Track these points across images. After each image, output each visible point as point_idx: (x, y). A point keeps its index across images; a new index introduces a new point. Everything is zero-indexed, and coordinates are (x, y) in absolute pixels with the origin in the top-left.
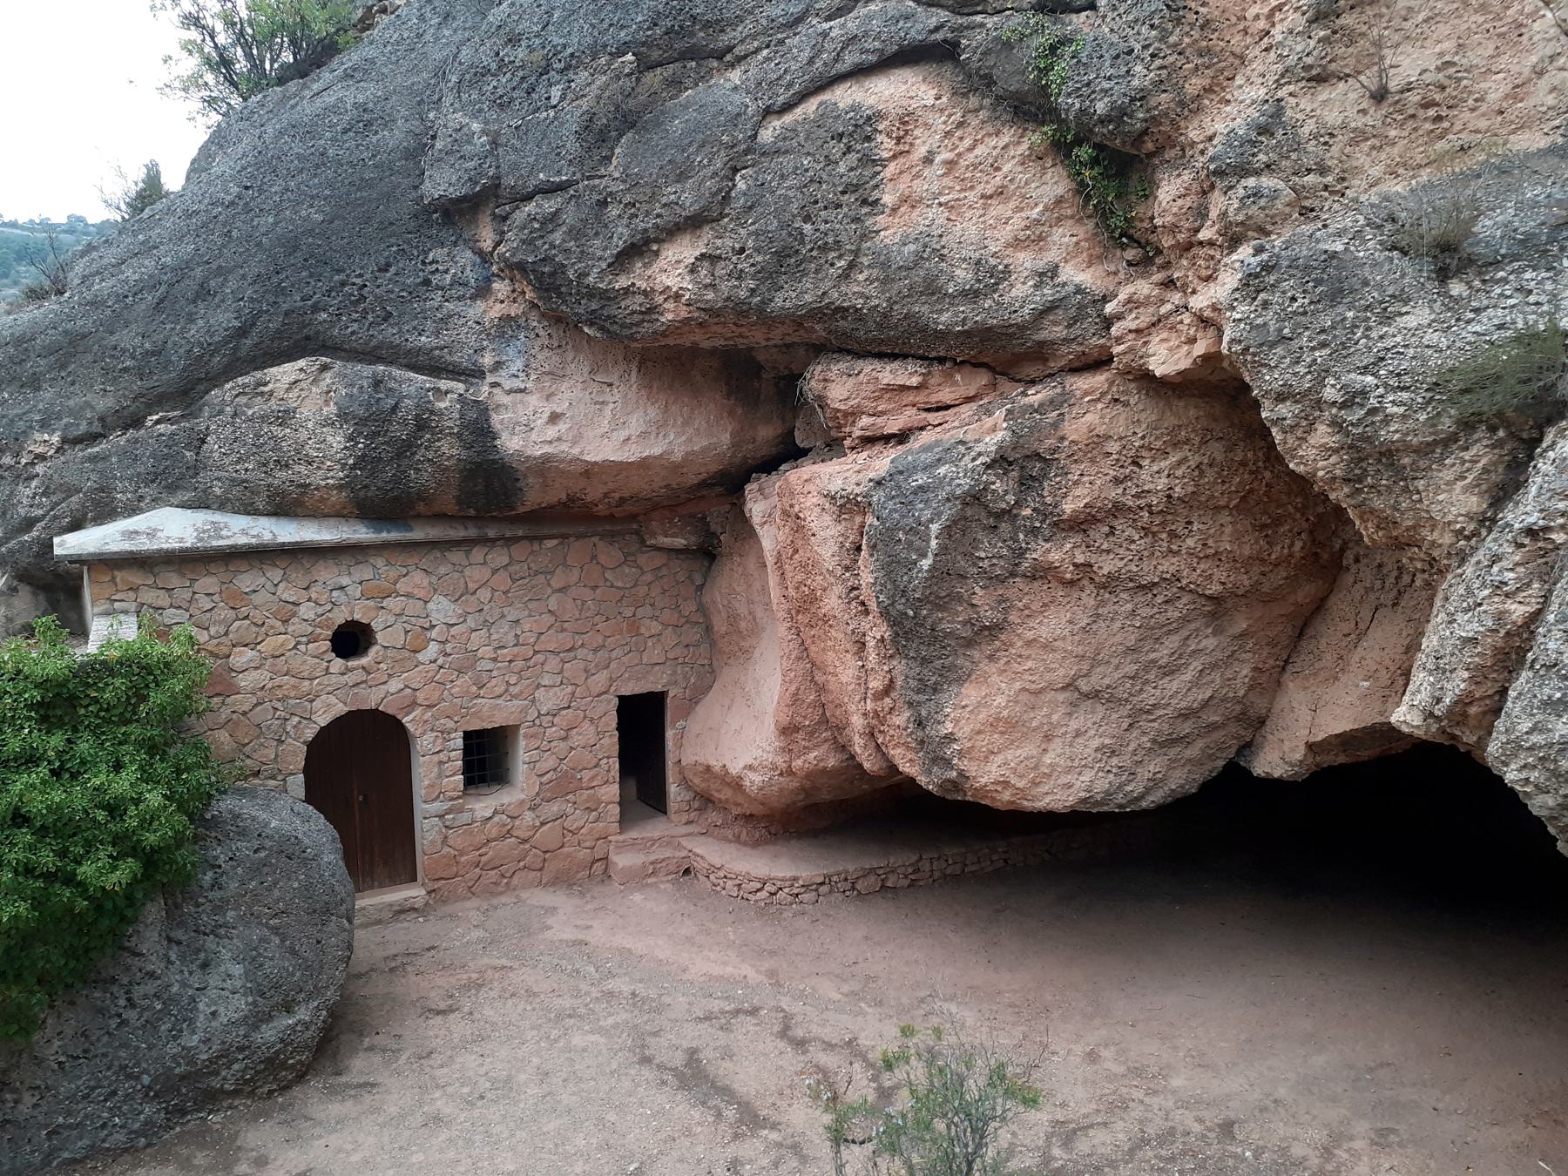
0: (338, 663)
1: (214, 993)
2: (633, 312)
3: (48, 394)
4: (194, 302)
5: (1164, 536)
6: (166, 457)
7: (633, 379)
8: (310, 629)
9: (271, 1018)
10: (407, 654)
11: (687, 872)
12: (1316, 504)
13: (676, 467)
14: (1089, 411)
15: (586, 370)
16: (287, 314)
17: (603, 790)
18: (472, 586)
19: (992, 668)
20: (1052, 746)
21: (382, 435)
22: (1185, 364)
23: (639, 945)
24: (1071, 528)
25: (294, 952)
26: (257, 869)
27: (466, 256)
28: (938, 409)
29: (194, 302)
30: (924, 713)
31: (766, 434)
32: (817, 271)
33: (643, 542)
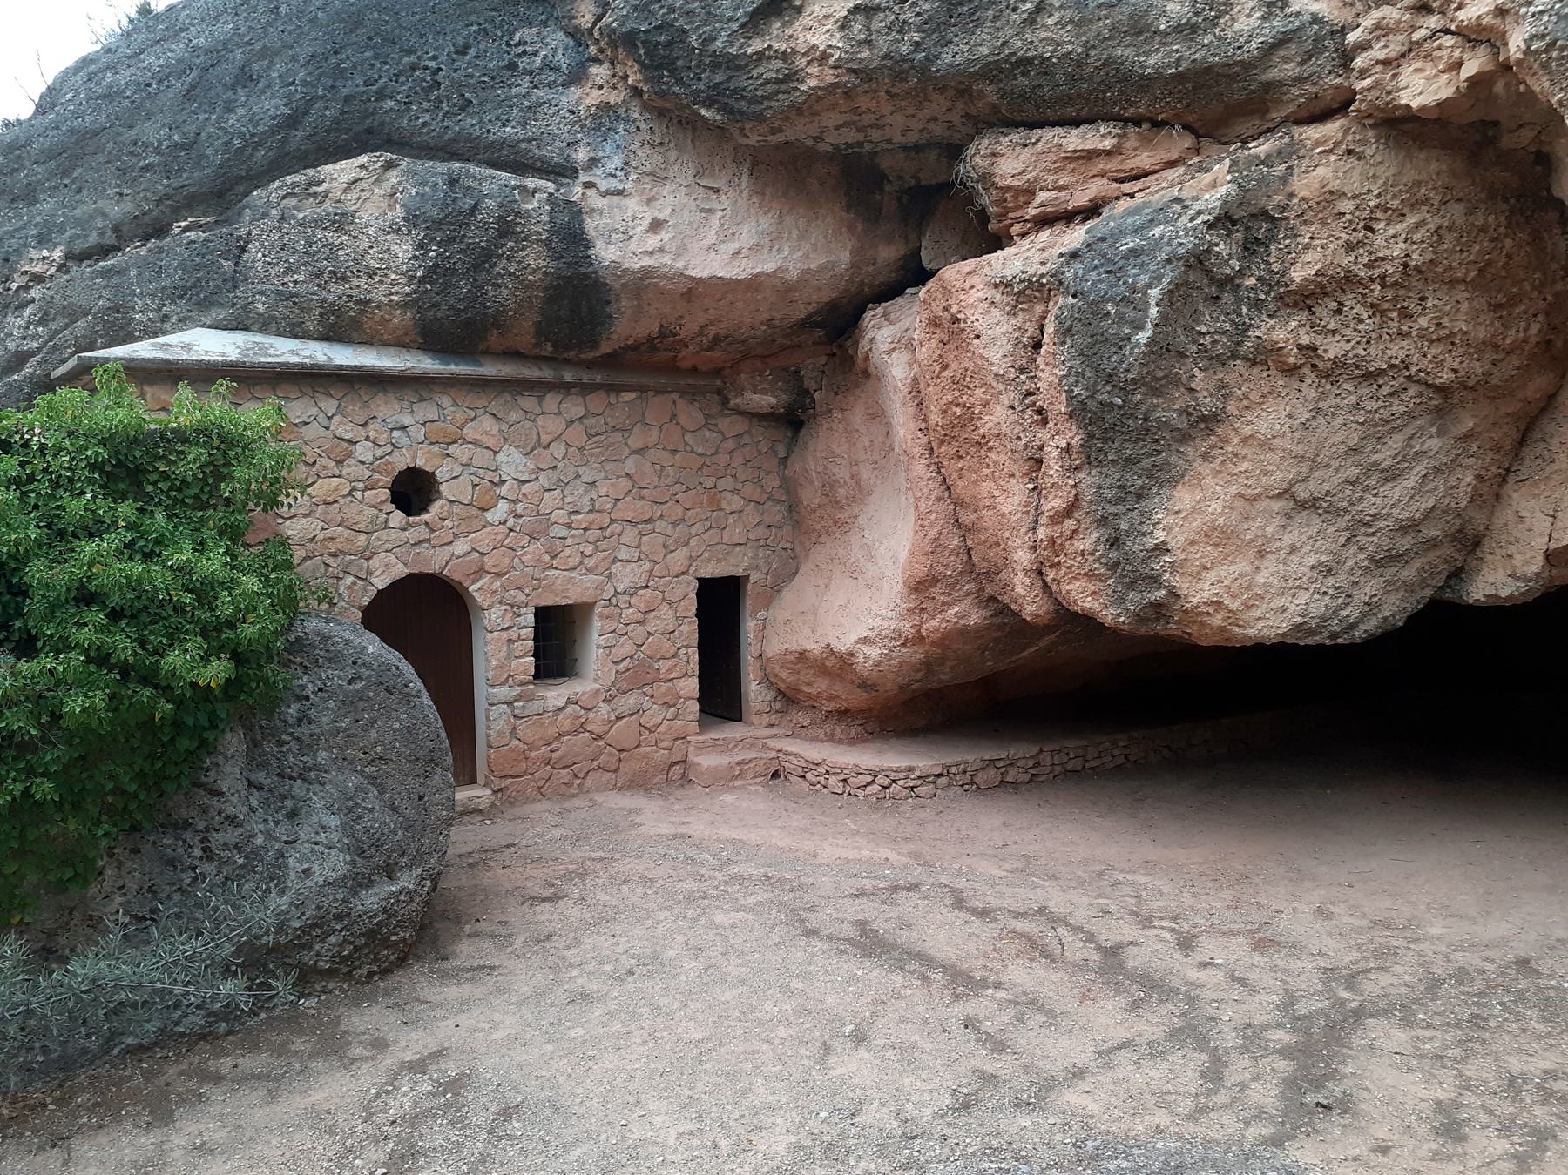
0: (398, 517)
1: (306, 848)
2: (768, 81)
3: (47, 205)
4: (233, 88)
5: (1394, 315)
6: (198, 268)
7: (744, 183)
8: (367, 473)
9: (370, 884)
10: (475, 511)
11: (776, 775)
12: (1554, 281)
13: (787, 290)
14: (1323, 166)
15: (691, 172)
16: (347, 100)
17: (683, 683)
18: (545, 438)
19: (1206, 469)
20: (1265, 563)
21: (459, 243)
22: (1446, 93)
23: (753, 837)
24: (1295, 305)
25: (394, 809)
26: (350, 704)
27: (557, 39)
28: (1137, 178)
29: (233, 88)
30: (1123, 526)
31: (888, 253)
32: (996, 19)
33: (725, 401)
